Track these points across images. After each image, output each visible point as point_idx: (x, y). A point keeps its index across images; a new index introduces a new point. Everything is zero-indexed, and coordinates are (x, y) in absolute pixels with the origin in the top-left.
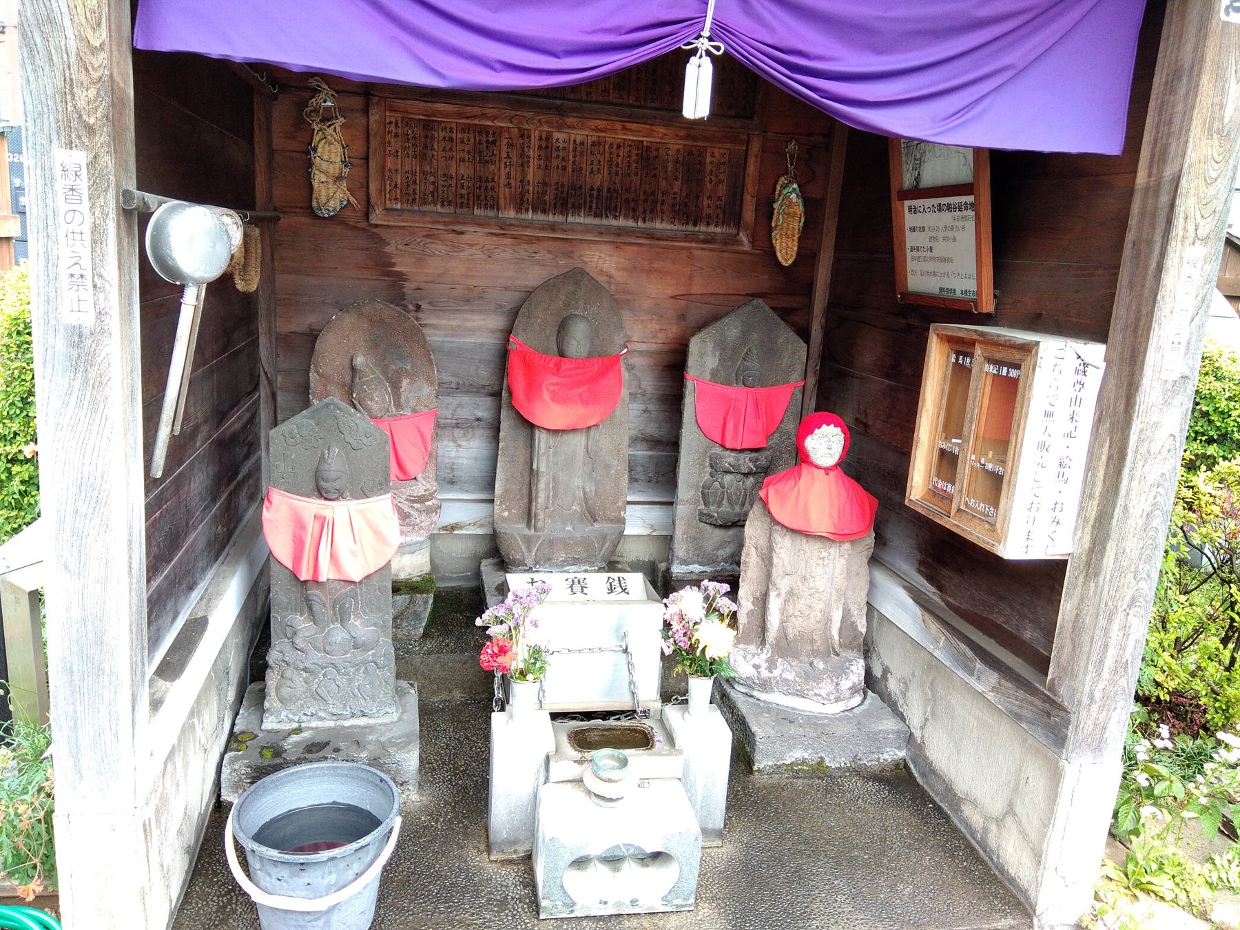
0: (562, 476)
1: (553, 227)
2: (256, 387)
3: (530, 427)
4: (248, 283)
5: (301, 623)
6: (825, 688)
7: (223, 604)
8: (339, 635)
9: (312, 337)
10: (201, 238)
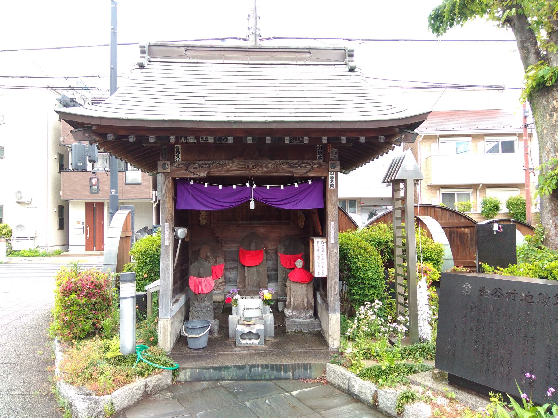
0: (251, 277)
1: (249, 224)
2: (188, 262)
3: (244, 266)
4: (187, 240)
5: (196, 303)
6: (303, 316)
7: (182, 299)
8: (203, 304)
9: (199, 250)
10: (181, 232)
